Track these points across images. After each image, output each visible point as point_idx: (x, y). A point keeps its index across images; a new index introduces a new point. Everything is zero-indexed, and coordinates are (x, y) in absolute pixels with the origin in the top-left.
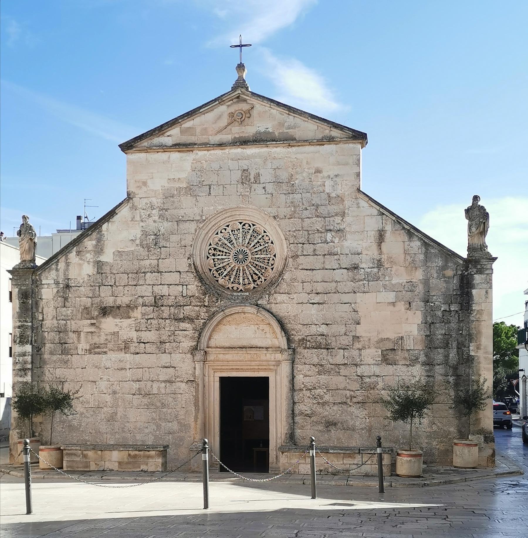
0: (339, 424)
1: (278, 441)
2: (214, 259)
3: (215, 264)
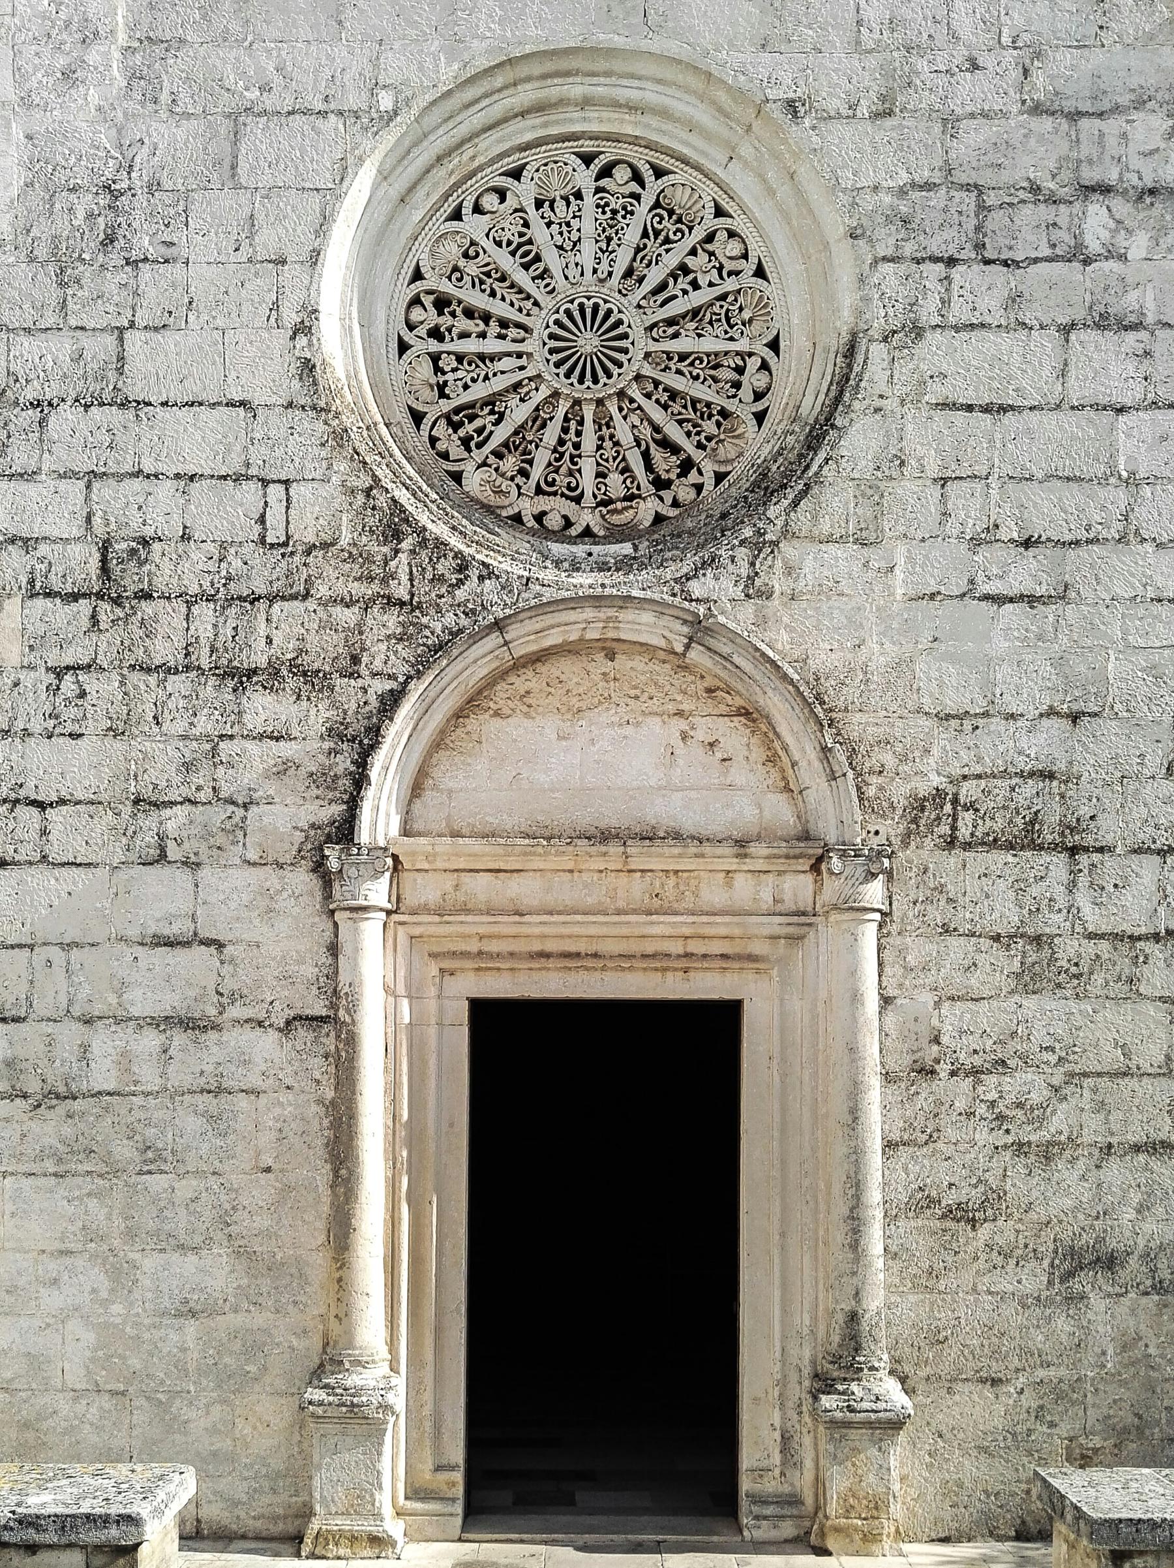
0: (1133, 1261)
1: (793, 1352)
2: (435, 358)
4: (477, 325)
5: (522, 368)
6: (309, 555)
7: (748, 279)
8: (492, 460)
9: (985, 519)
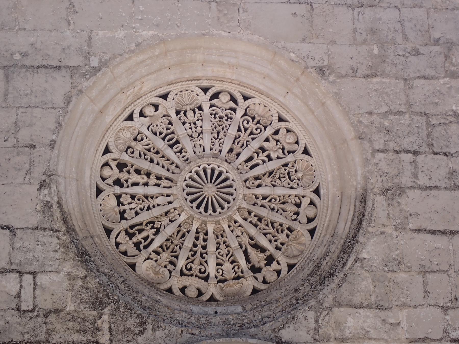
2: (118, 197)
3: (122, 214)
4: (143, 178)
5: (170, 203)
6: (47, 317)
8: (153, 256)
9: (449, 295)
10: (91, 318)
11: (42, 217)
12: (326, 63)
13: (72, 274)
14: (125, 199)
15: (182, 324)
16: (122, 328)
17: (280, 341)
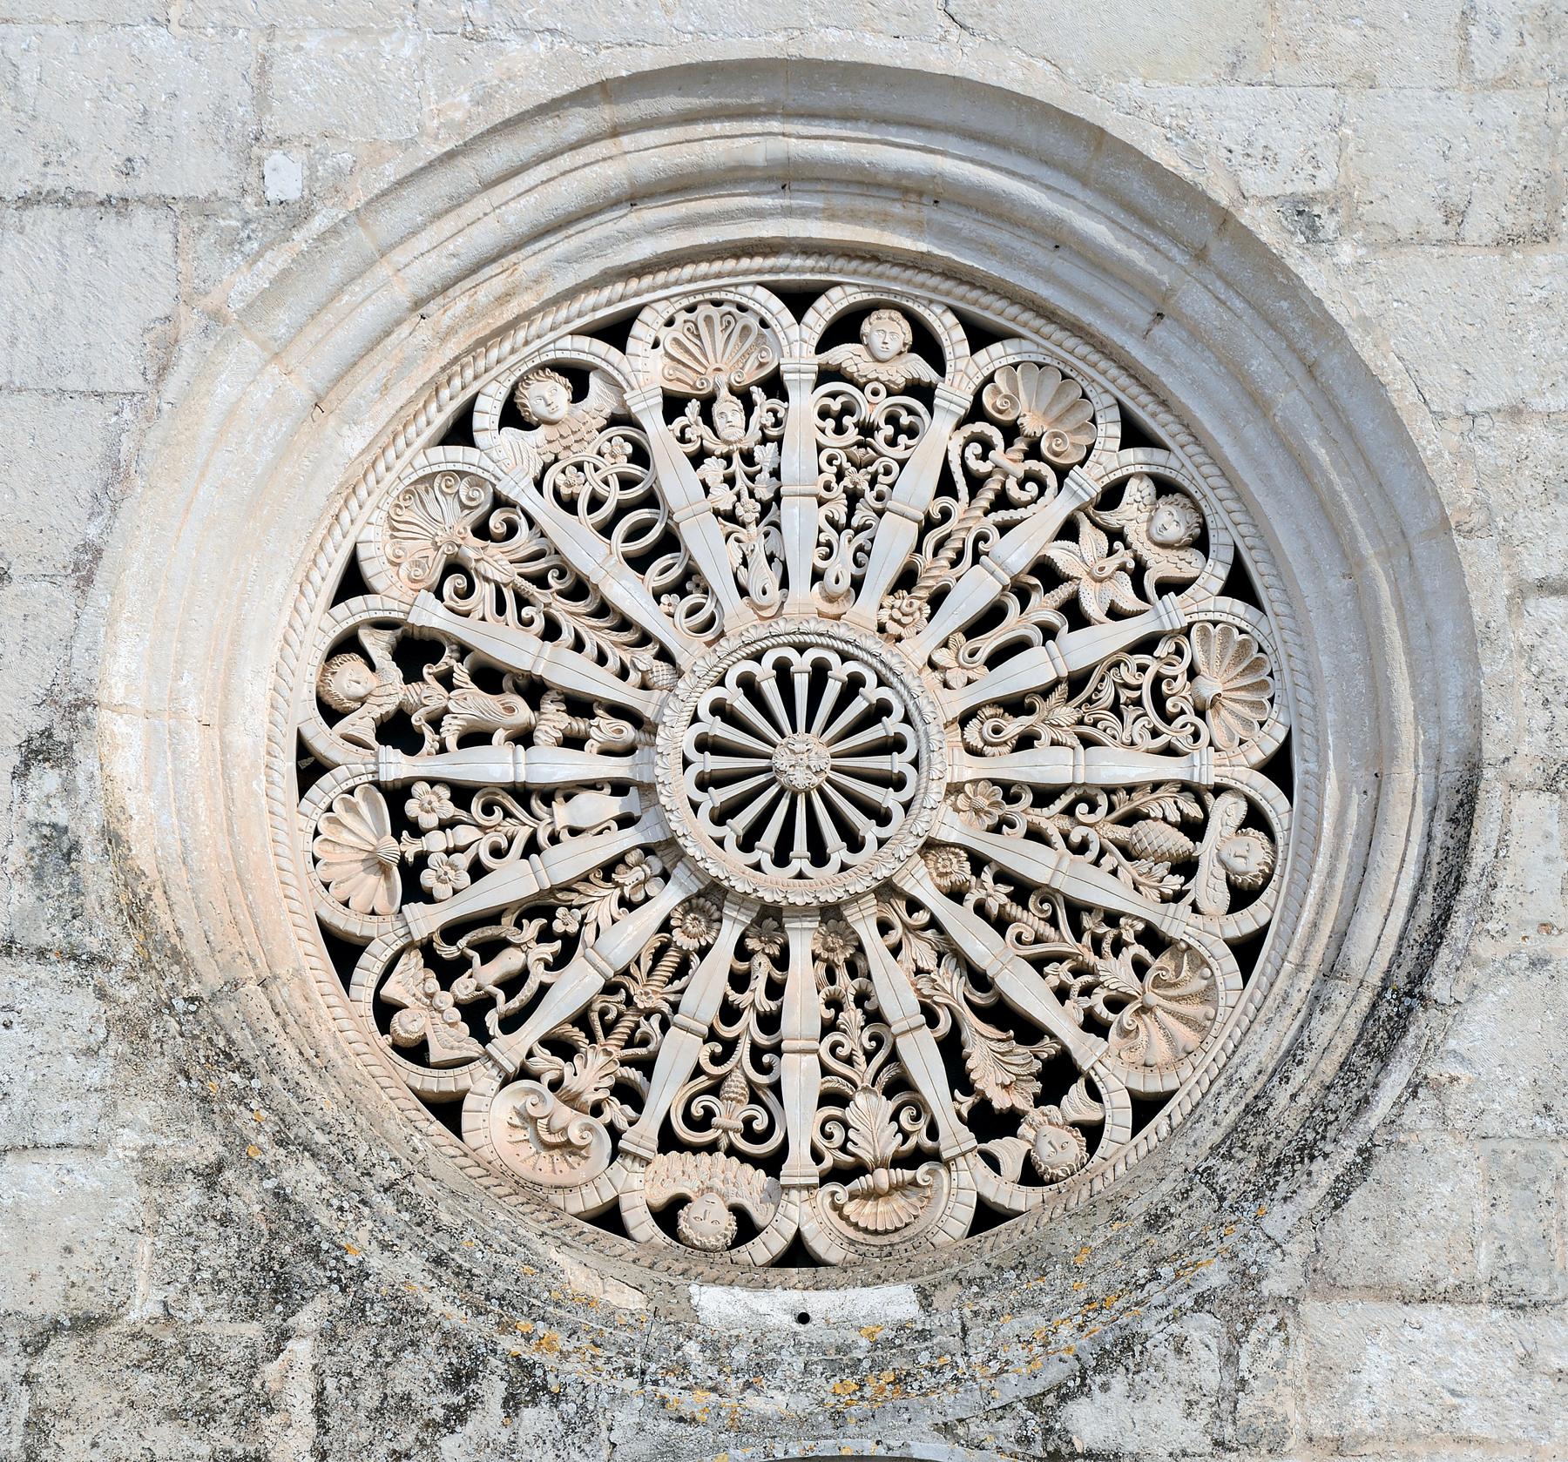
2: (397, 795)
6: (38, 1351)
7: (1207, 598)
8: (545, 1061)
10: (235, 1353)
11: (29, 899)
12: (1324, 181)
13: (160, 1157)
14: (428, 806)
15: (643, 1373)
16: (369, 1397)
17: (1065, 1450)
